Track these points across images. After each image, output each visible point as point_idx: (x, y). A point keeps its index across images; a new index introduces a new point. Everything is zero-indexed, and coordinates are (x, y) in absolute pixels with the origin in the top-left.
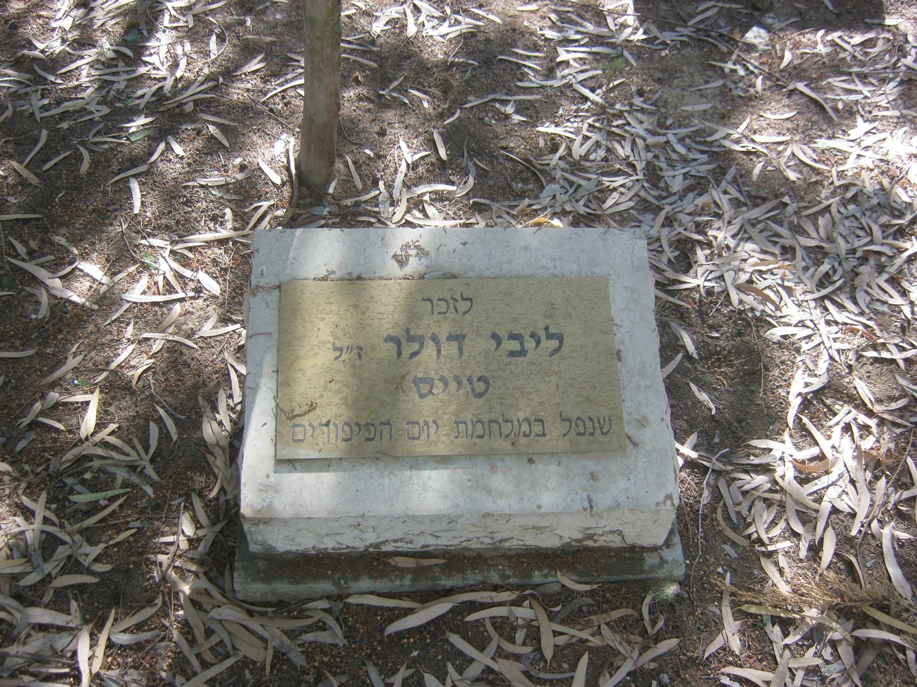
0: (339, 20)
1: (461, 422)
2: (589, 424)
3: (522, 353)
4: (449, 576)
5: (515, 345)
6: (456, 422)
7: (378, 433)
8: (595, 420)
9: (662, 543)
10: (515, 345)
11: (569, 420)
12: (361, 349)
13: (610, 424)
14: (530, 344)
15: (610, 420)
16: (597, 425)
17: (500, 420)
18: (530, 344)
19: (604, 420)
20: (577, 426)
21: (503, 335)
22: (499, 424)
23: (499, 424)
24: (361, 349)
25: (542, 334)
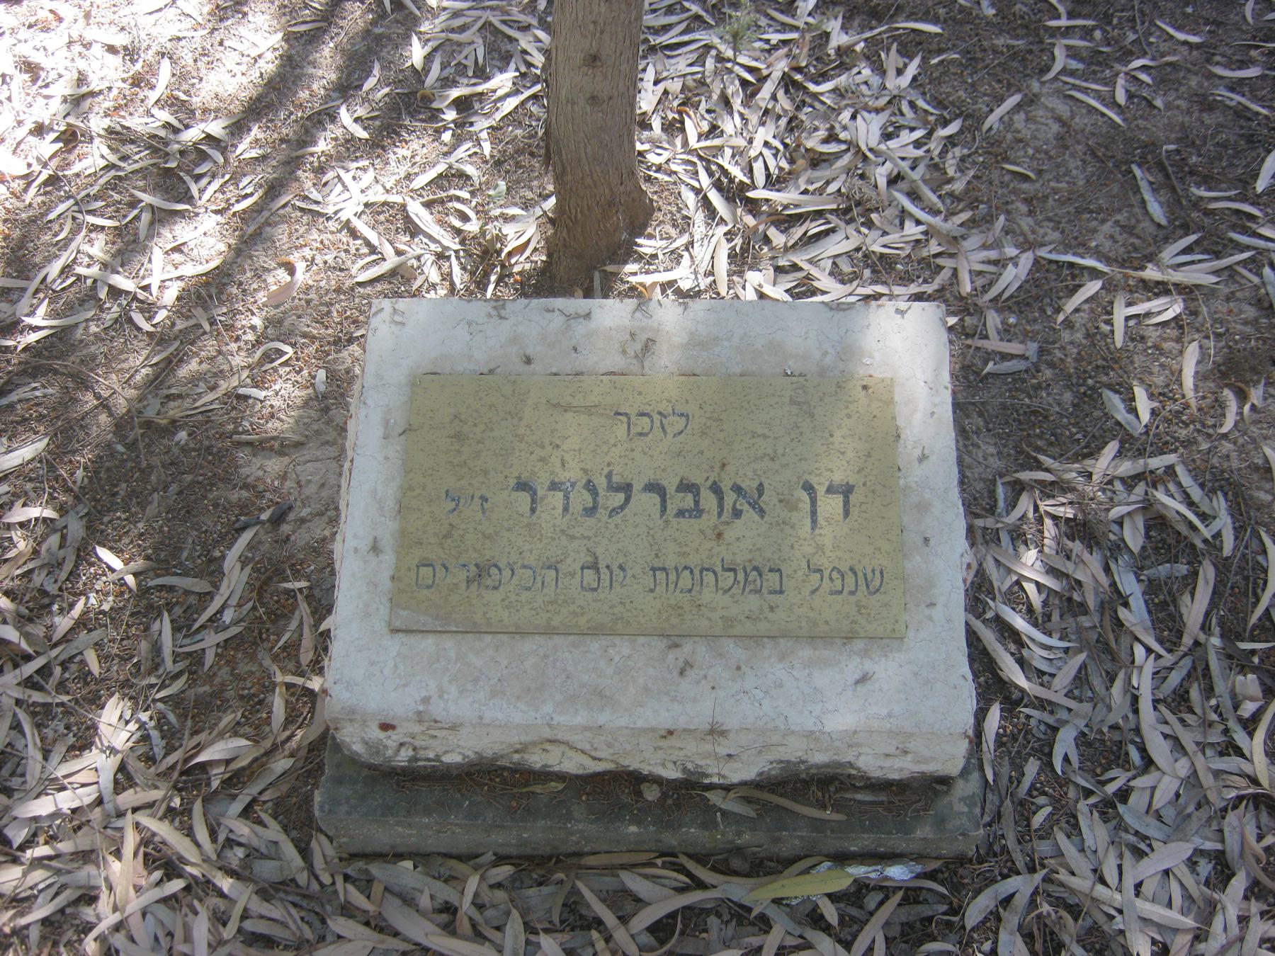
0: (558, 180)
1: (660, 569)
2: (850, 579)
3: (697, 511)
4: (1198, 188)
5: (688, 502)
6: (654, 569)
7: (539, 580)
8: (860, 574)
9: (961, 763)
10: (688, 502)
11: (819, 571)
12: (486, 500)
13: (882, 576)
14: (708, 500)
15: (882, 573)
16: (861, 581)
17: (719, 569)
18: (708, 500)
19: (873, 571)
20: (831, 579)
21: (671, 485)
22: (715, 573)
23: (715, 573)
24: (486, 500)
25: (601, 483)
